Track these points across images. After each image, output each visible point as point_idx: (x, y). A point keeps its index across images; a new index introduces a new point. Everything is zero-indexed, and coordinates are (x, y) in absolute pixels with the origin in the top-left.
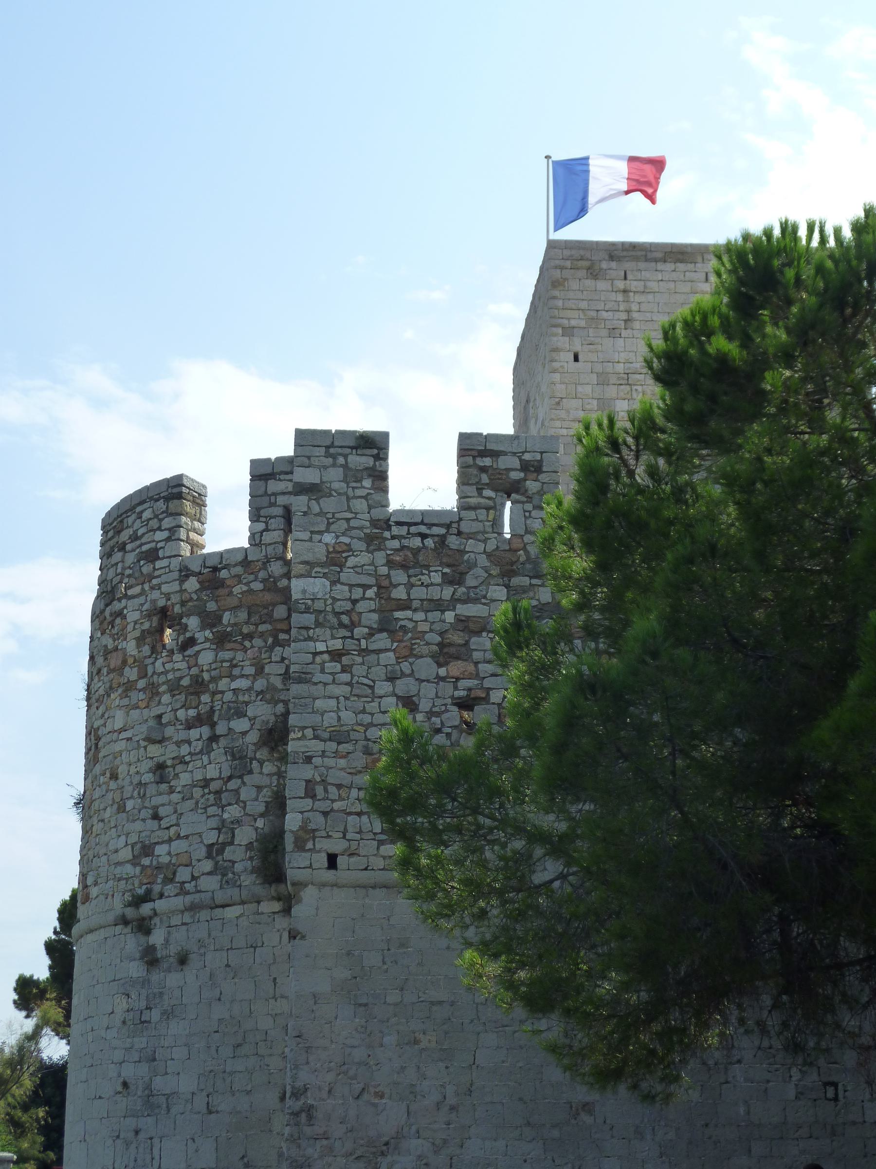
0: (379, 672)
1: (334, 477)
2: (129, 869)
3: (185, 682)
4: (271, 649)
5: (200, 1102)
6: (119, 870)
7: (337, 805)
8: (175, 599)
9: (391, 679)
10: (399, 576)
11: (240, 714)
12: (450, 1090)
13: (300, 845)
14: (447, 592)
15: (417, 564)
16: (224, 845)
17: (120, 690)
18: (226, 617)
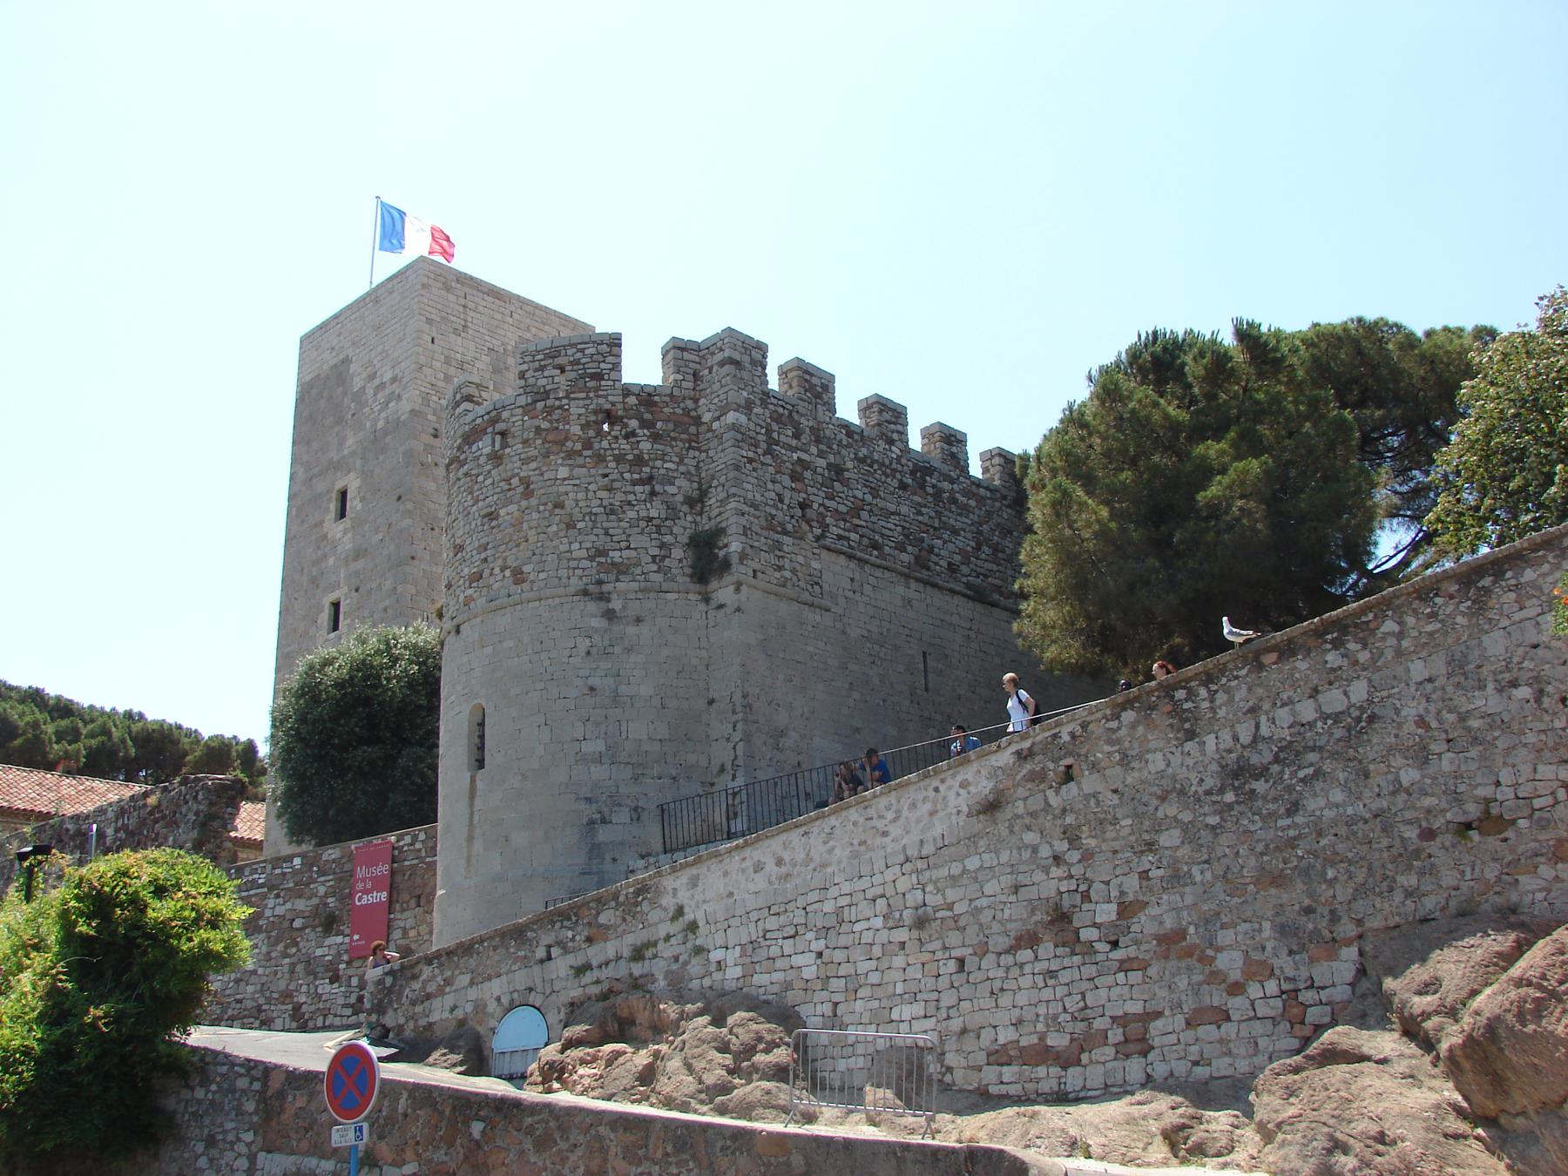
0: (768, 476)
2: (586, 564)
4: (688, 449)
5: (656, 702)
12: (806, 709)
16: (663, 558)
18: (659, 425)
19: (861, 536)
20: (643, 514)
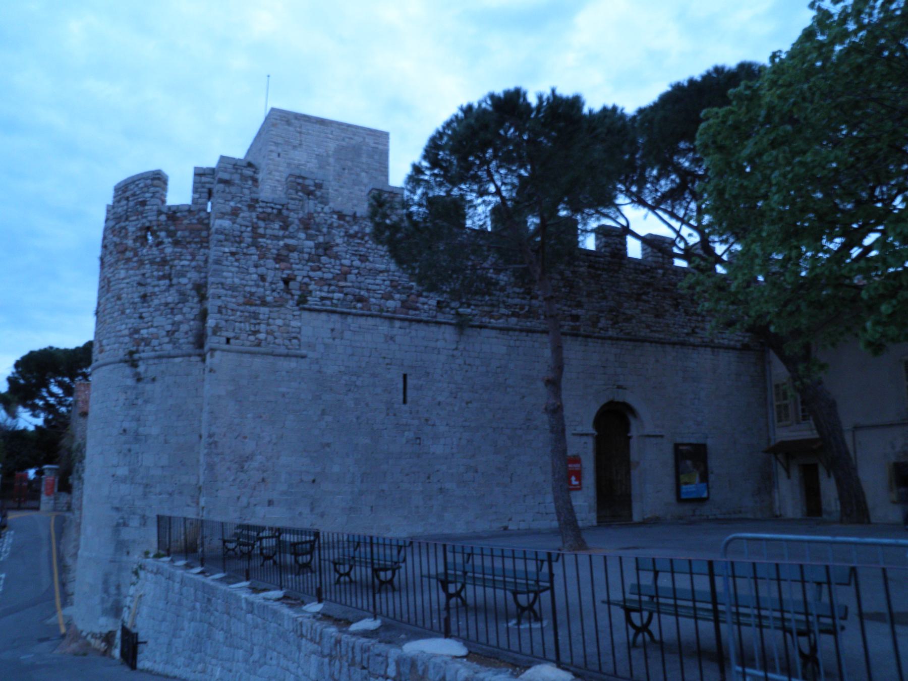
0: (250, 263)
1: (236, 178)
3: (158, 260)
6: (121, 339)
7: (232, 318)
8: (154, 223)
9: (256, 266)
10: (261, 224)
11: (184, 276)
12: (274, 436)
13: (214, 333)
14: (281, 233)
15: (269, 219)
16: (174, 332)
17: (123, 262)
18: (179, 233)
19: (346, 294)
20: (163, 301)
